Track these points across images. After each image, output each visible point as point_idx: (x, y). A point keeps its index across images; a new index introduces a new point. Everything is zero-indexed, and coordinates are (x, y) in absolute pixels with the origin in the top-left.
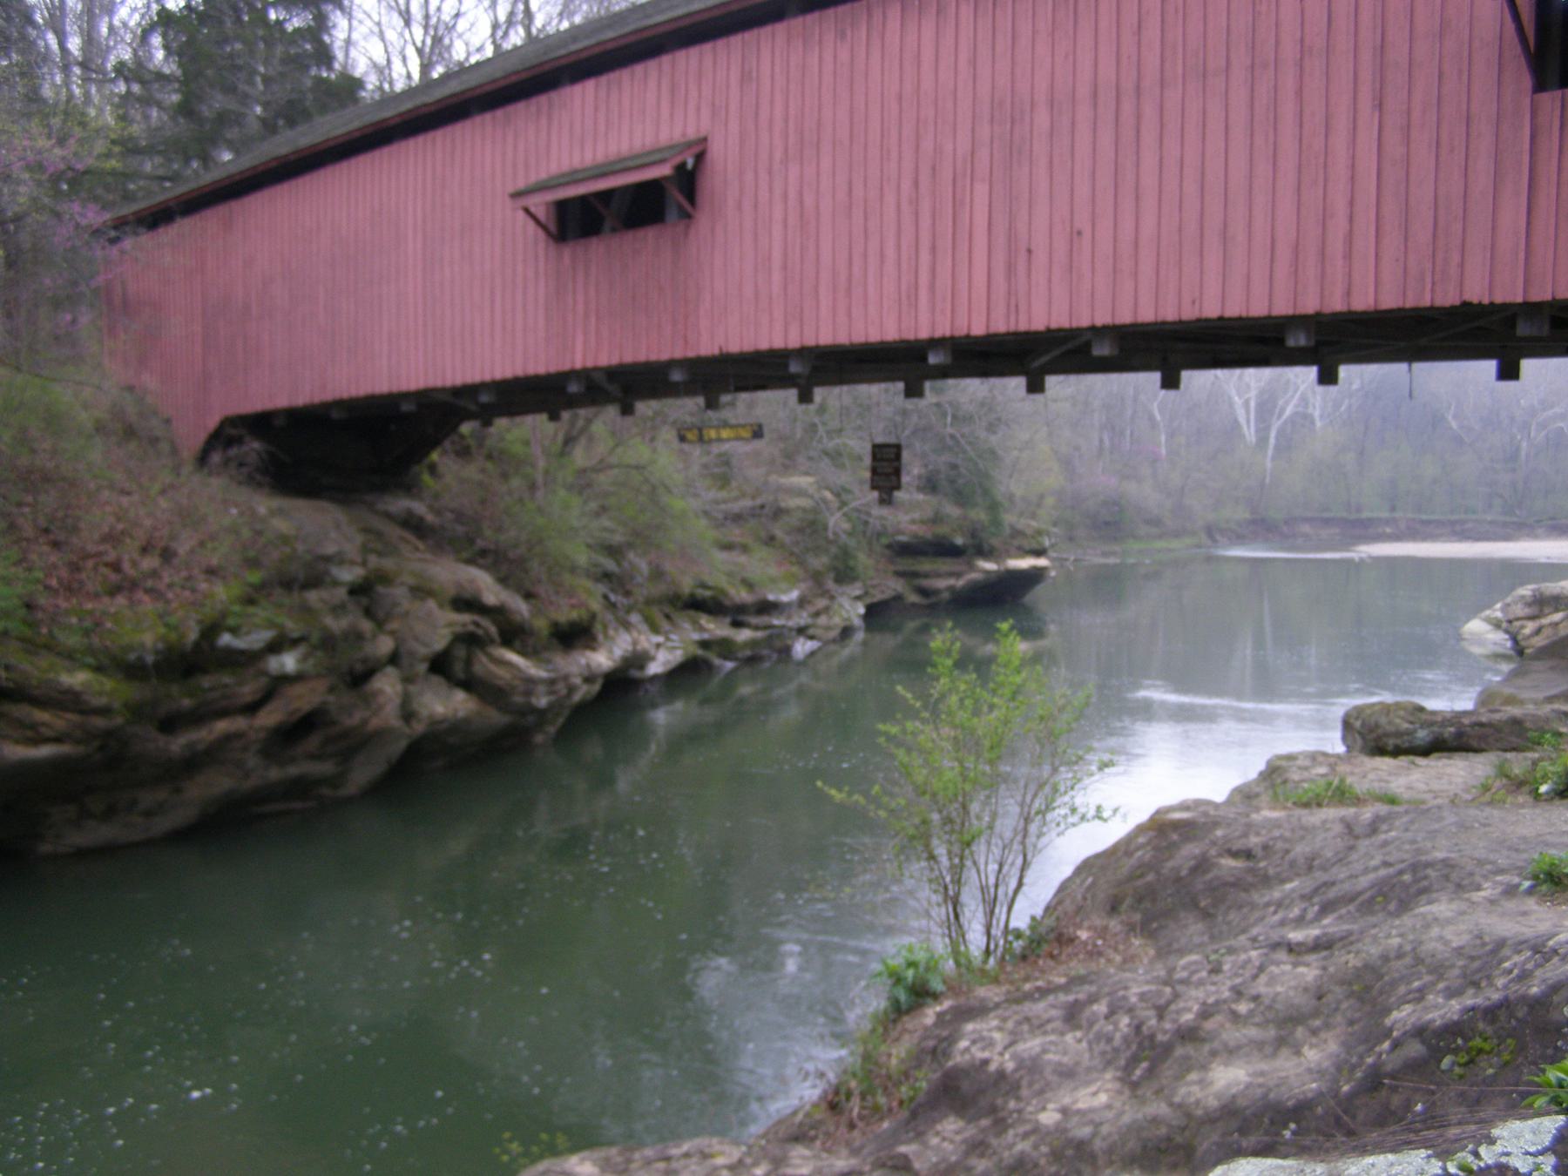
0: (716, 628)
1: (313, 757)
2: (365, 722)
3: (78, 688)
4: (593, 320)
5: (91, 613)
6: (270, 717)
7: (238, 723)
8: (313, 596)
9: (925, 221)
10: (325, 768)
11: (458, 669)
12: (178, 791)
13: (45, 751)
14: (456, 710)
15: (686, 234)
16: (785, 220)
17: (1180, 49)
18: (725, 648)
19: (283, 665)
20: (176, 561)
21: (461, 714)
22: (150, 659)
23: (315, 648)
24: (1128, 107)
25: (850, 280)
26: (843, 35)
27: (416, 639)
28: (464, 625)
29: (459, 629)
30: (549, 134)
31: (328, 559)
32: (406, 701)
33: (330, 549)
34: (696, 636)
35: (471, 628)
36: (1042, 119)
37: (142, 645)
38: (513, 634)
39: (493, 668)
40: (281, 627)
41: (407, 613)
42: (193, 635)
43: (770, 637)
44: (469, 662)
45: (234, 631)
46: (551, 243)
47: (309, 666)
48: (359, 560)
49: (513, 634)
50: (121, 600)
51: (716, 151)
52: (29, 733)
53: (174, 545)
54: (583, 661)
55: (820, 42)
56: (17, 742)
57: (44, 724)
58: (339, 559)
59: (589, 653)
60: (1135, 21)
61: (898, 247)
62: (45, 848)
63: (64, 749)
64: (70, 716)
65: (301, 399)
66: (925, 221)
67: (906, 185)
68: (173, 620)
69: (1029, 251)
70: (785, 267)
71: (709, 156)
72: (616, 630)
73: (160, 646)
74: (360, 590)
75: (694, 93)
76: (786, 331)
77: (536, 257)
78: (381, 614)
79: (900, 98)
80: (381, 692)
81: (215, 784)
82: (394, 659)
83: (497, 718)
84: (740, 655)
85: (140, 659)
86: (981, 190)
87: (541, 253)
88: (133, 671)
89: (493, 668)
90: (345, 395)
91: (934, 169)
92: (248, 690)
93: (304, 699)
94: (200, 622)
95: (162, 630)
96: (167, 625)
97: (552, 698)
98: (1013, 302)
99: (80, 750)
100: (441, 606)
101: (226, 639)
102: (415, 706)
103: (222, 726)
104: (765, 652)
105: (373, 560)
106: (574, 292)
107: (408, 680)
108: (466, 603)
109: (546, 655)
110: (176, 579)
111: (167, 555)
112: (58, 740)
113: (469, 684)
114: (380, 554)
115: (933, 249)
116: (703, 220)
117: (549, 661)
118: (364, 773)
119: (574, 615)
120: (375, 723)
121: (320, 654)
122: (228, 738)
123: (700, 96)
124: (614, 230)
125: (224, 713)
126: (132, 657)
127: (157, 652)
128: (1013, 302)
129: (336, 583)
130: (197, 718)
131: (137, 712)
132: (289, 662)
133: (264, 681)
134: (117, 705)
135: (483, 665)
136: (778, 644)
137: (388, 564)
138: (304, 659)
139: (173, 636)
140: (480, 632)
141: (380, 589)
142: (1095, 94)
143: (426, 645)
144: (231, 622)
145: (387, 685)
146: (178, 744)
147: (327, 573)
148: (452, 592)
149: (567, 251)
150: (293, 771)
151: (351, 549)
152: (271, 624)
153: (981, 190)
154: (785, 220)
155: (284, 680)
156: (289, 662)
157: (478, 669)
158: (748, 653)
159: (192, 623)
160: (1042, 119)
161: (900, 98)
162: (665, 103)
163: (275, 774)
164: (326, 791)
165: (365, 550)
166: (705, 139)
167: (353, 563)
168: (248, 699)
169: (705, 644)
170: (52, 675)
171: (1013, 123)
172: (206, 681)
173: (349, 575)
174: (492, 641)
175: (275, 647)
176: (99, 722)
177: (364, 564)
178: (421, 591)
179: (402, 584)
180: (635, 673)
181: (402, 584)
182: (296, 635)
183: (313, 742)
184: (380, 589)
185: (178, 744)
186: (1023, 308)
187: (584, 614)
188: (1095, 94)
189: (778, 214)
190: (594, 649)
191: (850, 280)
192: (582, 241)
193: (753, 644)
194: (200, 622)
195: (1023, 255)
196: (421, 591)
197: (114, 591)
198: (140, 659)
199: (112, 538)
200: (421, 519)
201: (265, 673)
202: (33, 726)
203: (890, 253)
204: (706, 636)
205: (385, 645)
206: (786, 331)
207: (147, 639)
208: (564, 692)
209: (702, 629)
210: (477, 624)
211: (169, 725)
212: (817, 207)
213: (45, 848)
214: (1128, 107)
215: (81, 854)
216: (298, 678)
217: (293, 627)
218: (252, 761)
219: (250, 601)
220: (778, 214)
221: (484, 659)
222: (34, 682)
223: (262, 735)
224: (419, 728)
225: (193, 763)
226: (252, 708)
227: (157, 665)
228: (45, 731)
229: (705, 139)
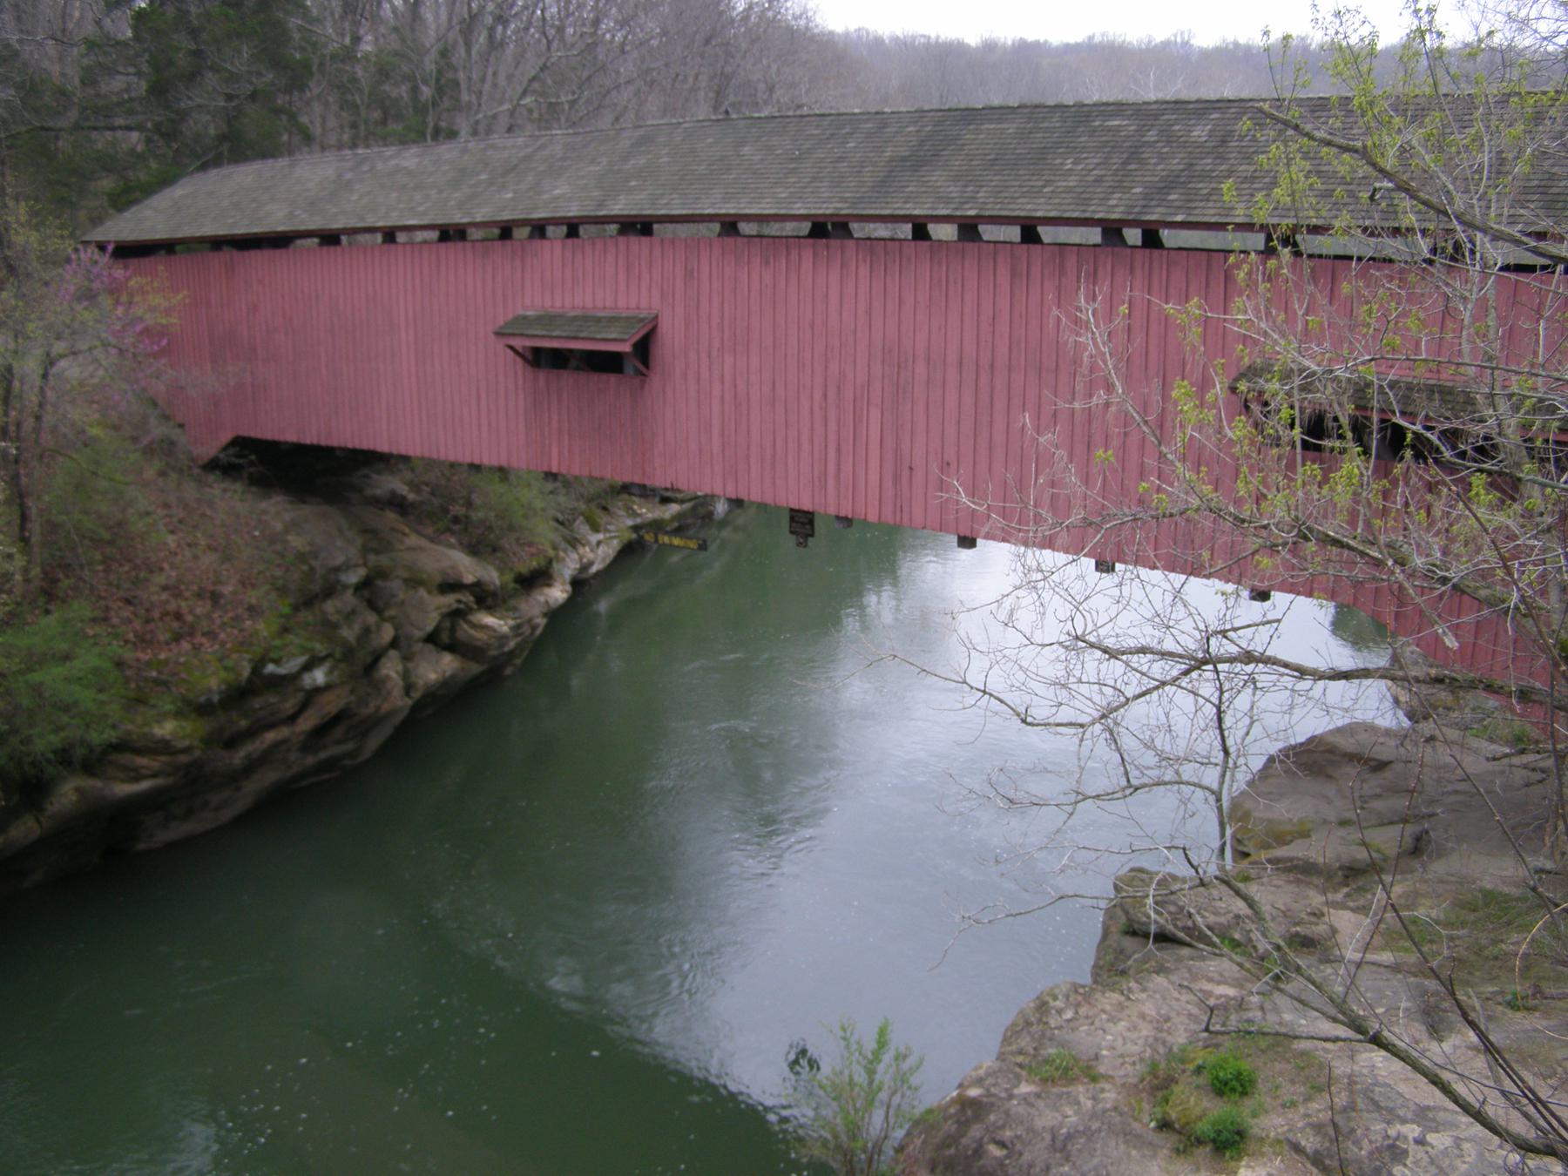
0: (648, 512)
1: (339, 742)
2: (378, 708)
3: (168, 737)
4: (566, 437)
5: (166, 662)
6: (306, 723)
7: (282, 733)
8: (330, 607)
9: (832, 426)
10: (349, 746)
11: (445, 637)
12: (238, 789)
13: (145, 785)
14: (444, 672)
15: (642, 387)
16: (722, 398)
17: (1023, 345)
18: (657, 526)
19: (315, 680)
20: (222, 601)
21: (448, 674)
22: (216, 698)
23: (339, 661)
24: (984, 378)
25: (774, 456)
26: (767, 263)
27: (412, 625)
28: (450, 605)
29: (445, 610)
30: (523, 271)
31: (337, 569)
32: (406, 675)
33: (339, 560)
34: (630, 522)
35: (455, 606)
36: (921, 370)
37: (210, 690)
38: (485, 598)
39: (472, 632)
40: (312, 650)
41: (403, 602)
42: (246, 672)
43: (694, 508)
44: (453, 630)
45: (277, 662)
46: (529, 368)
47: (335, 676)
48: (361, 561)
49: (485, 598)
50: (185, 645)
51: (665, 327)
52: (132, 774)
53: (220, 588)
54: (542, 599)
55: (749, 263)
56: (123, 781)
57: (143, 767)
58: (347, 567)
59: (547, 590)
60: (991, 312)
61: (812, 441)
62: (141, 846)
63: (160, 781)
64: (163, 758)
65: (310, 438)
66: (832, 426)
67: (818, 396)
68: (229, 663)
69: (911, 468)
70: (722, 434)
71: (659, 330)
72: (565, 551)
73: (223, 687)
74: (366, 584)
75: (645, 275)
76: (724, 485)
77: (516, 373)
78: (381, 604)
79: (812, 325)
80: (387, 676)
81: (268, 777)
82: (394, 644)
83: (475, 668)
84: (668, 529)
85: (209, 700)
86: (875, 414)
87: (520, 373)
88: (204, 710)
89: (472, 632)
90: (350, 446)
91: (839, 387)
92: (289, 705)
93: (331, 704)
94: (250, 661)
95: (223, 674)
96: (226, 669)
97: (519, 639)
98: (899, 505)
99: (171, 780)
100: (430, 592)
101: (270, 668)
102: (413, 679)
103: (271, 736)
104: (690, 521)
105: (372, 558)
106: (549, 409)
107: (406, 658)
108: (450, 586)
109: (512, 602)
110: (225, 619)
111: (215, 598)
112: (154, 776)
113: (452, 647)
114: (377, 552)
115: (839, 450)
116: (655, 380)
117: (515, 609)
118: (375, 741)
119: (534, 564)
120: (386, 707)
121: (343, 666)
122: (276, 745)
123: (651, 279)
124: (578, 369)
125: (272, 726)
126: (202, 699)
127: (220, 692)
128: (899, 505)
129: (345, 587)
130: (252, 733)
131: (208, 741)
132: (319, 676)
133: (301, 696)
134: (196, 743)
135: (465, 631)
136: (702, 511)
137: (384, 560)
138: (330, 672)
139: (231, 677)
140: (462, 606)
141: (379, 583)
142: (961, 364)
143: (419, 629)
144: (274, 655)
145: (391, 668)
146: (239, 757)
147: (338, 582)
148: (438, 579)
149: (542, 375)
150: (323, 755)
151: (353, 553)
152: (304, 650)
153: (875, 414)
154: (722, 398)
155: (317, 691)
156: (319, 676)
157: (460, 635)
158: (676, 524)
159: (245, 664)
160: (921, 370)
161: (812, 325)
162: (622, 277)
163: (310, 760)
164: (347, 762)
165: (365, 550)
166: (656, 317)
167: (356, 566)
168: (291, 712)
169: (636, 528)
170: (146, 730)
171: (899, 367)
172: (257, 703)
173: (353, 578)
174: (471, 609)
175: (308, 667)
176: (184, 758)
177: (365, 564)
178: (414, 582)
179: (398, 577)
180: (584, 576)
181: (398, 577)
182: (324, 653)
183: (339, 732)
184: (379, 583)
185: (239, 757)
186: (906, 508)
187: (543, 562)
188: (961, 364)
189: (716, 392)
190: (550, 586)
191: (774, 456)
192: (555, 371)
193: (679, 516)
194: (250, 661)
195: (906, 472)
196: (414, 582)
197: (177, 638)
198: (209, 700)
199: (174, 590)
200: (404, 498)
201: (302, 689)
202: (136, 769)
203: (806, 446)
204: (639, 521)
205: (388, 633)
206: (724, 485)
207: (213, 683)
208: (529, 631)
209: (635, 514)
210: (459, 601)
211: (232, 743)
212: (748, 394)
213: (141, 846)
214: (984, 378)
215: (170, 846)
216: (327, 687)
217: (321, 648)
218: (293, 756)
219: (285, 630)
220: (716, 392)
221: (465, 627)
222: (135, 737)
223: (302, 738)
224: (416, 695)
225: (251, 767)
226: (292, 719)
227: (221, 702)
228: (144, 772)
229: (656, 317)
